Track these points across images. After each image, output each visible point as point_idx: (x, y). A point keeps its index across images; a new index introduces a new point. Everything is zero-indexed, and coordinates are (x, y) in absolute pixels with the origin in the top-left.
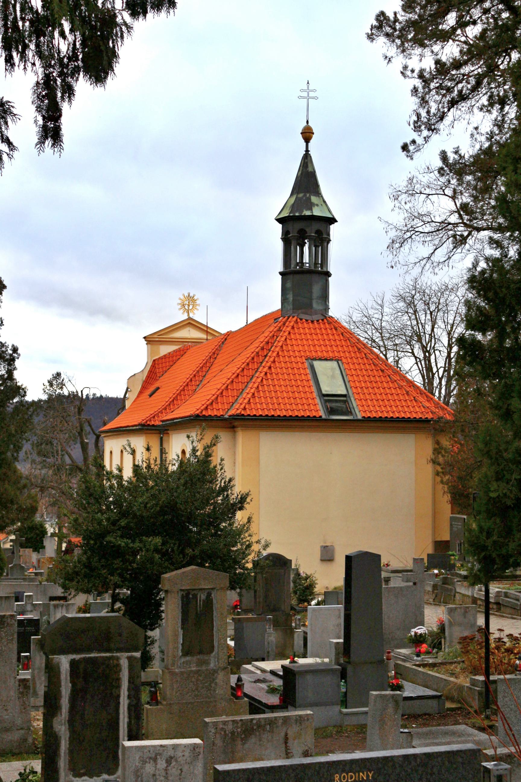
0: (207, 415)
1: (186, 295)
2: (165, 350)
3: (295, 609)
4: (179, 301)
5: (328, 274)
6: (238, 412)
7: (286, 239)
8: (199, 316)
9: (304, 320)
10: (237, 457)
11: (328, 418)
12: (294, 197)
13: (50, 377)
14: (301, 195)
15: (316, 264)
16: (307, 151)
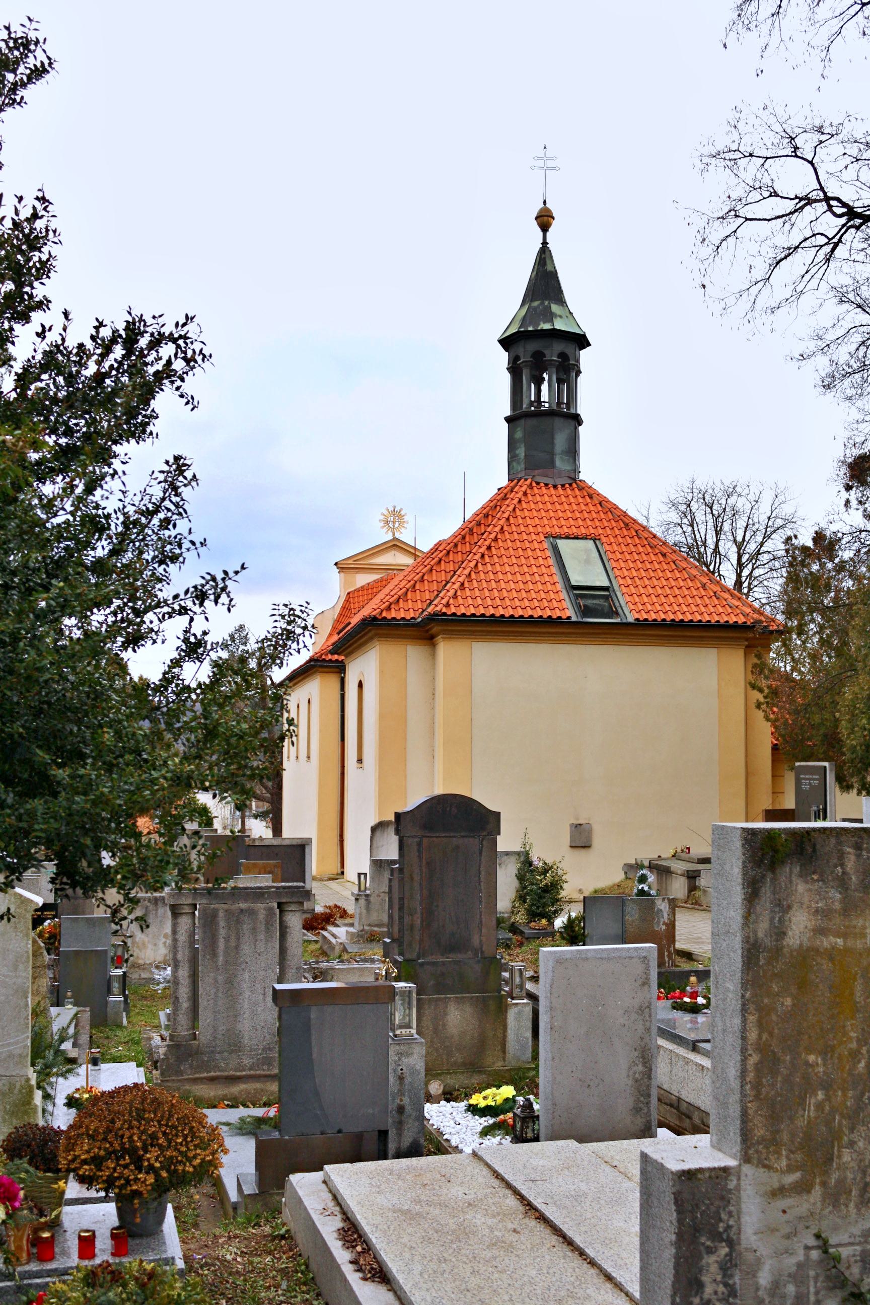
0: (389, 617)
1: (391, 509)
2: (363, 579)
3: (522, 933)
4: (382, 517)
5: (577, 420)
6: (438, 609)
7: (514, 369)
8: (406, 536)
9: (542, 484)
10: (436, 683)
11: (580, 620)
12: (526, 307)
13: (231, 630)
14: (536, 304)
15: (559, 403)
16: (545, 243)
